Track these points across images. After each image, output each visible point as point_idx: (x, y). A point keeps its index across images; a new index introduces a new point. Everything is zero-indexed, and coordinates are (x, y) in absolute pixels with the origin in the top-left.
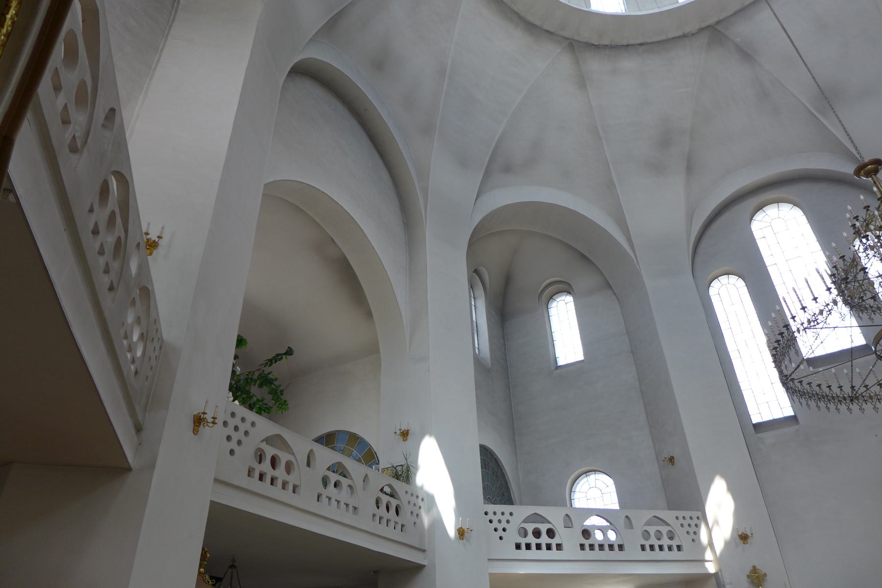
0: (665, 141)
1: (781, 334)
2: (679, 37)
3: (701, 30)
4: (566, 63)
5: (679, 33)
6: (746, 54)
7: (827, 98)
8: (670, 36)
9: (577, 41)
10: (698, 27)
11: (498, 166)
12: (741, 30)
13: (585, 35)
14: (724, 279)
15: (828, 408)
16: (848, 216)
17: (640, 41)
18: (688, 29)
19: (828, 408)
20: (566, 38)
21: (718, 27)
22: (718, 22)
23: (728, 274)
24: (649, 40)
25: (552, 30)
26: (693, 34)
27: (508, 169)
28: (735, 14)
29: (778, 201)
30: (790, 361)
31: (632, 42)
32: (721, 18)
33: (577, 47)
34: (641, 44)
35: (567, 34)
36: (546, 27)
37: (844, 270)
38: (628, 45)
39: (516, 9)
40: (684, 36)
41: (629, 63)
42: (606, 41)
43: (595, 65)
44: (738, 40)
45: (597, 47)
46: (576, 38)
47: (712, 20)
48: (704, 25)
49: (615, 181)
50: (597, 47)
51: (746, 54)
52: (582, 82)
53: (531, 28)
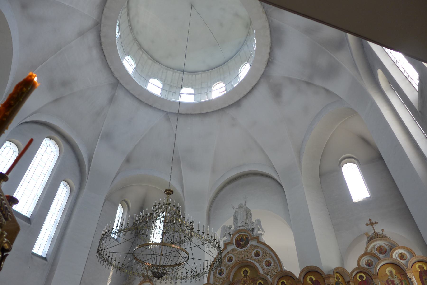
0: (65, 84)
1: (109, 230)
2: (111, 71)
4: (89, 23)
6: (112, 100)
7: (107, 136)
8: (111, 67)
9: (100, 26)
10: (117, 76)
12: (120, 93)
13: (104, 30)
14: (13, 145)
15: (106, 266)
17: (106, 55)
18: (115, 73)
19: (106, 266)
20: (101, 21)
21: (119, 84)
22: (121, 84)
23: (16, 145)
24: (107, 59)
28: (126, 89)
29: (57, 143)
30: (106, 241)
31: (105, 52)
33: (98, 26)
34: (104, 56)
35: (103, 20)
36: (105, 10)
38: (103, 50)
40: (112, 73)
41: (95, 53)
42: (103, 40)
43: (91, 38)
44: (116, 94)
45: (99, 36)
46: (102, 25)
47: (121, 81)
48: (119, 79)
50: (99, 36)
51: (112, 100)
52: (81, 34)
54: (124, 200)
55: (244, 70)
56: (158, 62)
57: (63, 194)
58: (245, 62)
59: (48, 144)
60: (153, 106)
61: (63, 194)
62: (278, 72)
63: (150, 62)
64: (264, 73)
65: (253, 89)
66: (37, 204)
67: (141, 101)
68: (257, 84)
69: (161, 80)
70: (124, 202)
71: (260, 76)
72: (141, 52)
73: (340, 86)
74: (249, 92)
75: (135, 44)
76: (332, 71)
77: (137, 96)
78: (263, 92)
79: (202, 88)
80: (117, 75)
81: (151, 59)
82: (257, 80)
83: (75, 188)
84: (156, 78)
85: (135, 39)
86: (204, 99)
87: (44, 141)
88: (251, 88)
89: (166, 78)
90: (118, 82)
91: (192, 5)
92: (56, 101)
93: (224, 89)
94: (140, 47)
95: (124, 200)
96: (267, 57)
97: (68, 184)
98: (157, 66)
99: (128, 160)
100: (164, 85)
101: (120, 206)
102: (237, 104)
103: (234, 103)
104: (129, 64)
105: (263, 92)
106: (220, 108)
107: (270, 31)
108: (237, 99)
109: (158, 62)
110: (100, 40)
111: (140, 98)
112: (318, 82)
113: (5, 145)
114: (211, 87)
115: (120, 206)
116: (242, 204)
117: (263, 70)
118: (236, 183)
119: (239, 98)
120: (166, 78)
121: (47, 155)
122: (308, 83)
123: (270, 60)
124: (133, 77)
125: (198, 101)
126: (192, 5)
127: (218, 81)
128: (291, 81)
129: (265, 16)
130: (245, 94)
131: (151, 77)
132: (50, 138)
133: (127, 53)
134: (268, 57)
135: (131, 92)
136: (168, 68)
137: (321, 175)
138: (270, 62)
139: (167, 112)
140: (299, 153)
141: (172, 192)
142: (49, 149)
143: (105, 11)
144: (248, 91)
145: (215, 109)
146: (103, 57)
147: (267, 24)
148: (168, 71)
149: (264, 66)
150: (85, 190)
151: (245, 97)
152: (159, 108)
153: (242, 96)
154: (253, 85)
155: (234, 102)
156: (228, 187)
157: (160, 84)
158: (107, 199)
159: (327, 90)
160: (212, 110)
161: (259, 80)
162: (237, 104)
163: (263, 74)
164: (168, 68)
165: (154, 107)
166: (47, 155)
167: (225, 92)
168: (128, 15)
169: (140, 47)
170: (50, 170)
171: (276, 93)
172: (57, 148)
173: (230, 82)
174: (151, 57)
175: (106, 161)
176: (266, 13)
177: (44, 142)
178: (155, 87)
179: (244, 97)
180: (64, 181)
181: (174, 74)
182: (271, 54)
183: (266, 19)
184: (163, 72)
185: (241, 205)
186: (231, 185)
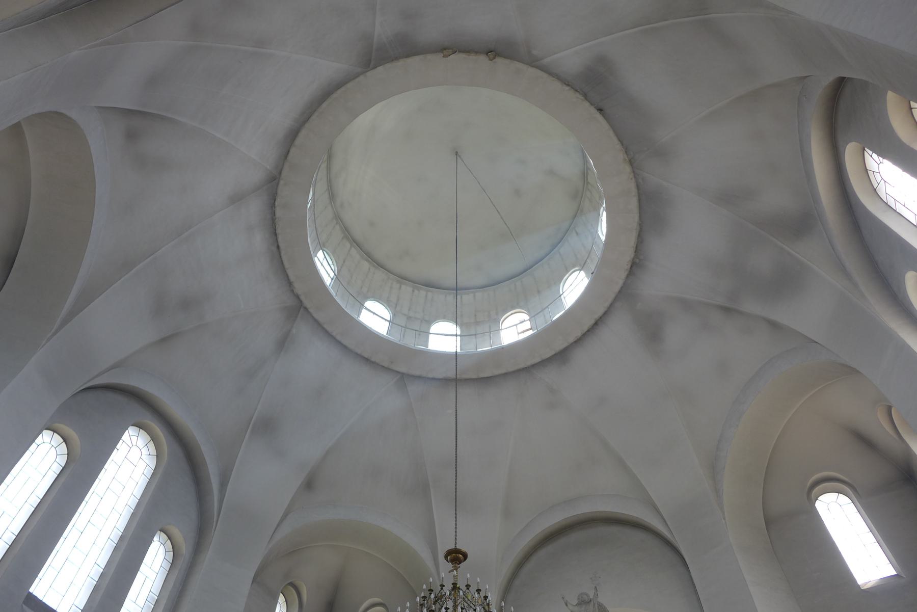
3: (298, 297)
5: (292, 278)
6: (283, 343)
9: (278, 184)
11: (136, 123)
13: (284, 192)
14: (57, 439)
16: (425, 587)
17: (281, 245)
20: (280, 173)
21: (302, 309)
22: (306, 309)
23: (65, 441)
24: (282, 254)
25: (289, 158)
26: (293, 291)
27: (131, 136)
28: (316, 320)
29: (154, 438)
31: (280, 238)
32: (311, 310)
33: (272, 183)
34: (278, 247)
35: (285, 173)
36: (293, 150)
37: (436, 597)
38: (276, 235)
39: (313, 117)
40: (290, 283)
41: (259, 240)
42: (279, 213)
43: (254, 208)
44: (294, 331)
46: (282, 182)
47: (306, 303)
48: (302, 298)
49: (133, 271)
50: (272, 206)
51: (283, 343)
52: (237, 199)
53: (293, 135)
54: (292, 584)
55: (574, 286)
56: (380, 265)
57: (156, 559)
58: (574, 267)
59: (134, 439)
60: (373, 360)
61: (156, 559)
62: (656, 286)
63: (366, 265)
64: (622, 288)
65: (596, 324)
66: (96, 589)
67: (345, 347)
68: (606, 313)
69: (387, 303)
70: (292, 588)
71: (613, 296)
72: (348, 245)
73: (808, 314)
74: (588, 331)
75: (338, 227)
76: (786, 281)
77: (338, 338)
78: (620, 329)
79: (477, 323)
80: (299, 288)
81: (367, 260)
82: (607, 304)
83: (186, 549)
84: (379, 299)
85: (338, 218)
86: (485, 348)
87: (126, 434)
88: (593, 322)
89: (398, 300)
90: (302, 306)
91: (457, 153)
92: (164, 340)
93: (528, 325)
94: (347, 234)
95: (292, 584)
96: (629, 255)
97: (169, 538)
98: (380, 275)
99: (309, 485)
100: (394, 315)
101: (281, 599)
102: (561, 357)
103: (555, 353)
104: (325, 267)
105: (620, 329)
106: (522, 366)
107: (640, 201)
108: (560, 345)
109: (380, 265)
110: (274, 214)
111: (346, 342)
112: (751, 306)
113: (39, 440)
114: (497, 321)
115: (281, 599)
116: (586, 594)
117: (621, 282)
118: (562, 541)
119: (565, 345)
120: (398, 300)
121: (131, 464)
122: (727, 310)
123: (637, 261)
124: (334, 294)
125: (542, 325)
126: (457, 153)
127: (513, 308)
128: (686, 305)
129: (628, 169)
130: (579, 334)
131: (367, 298)
132: (140, 426)
133: (322, 246)
134: (632, 256)
135: (325, 326)
136: (403, 279)
137: (769, 522)
138: (636, 266)
139: (403, 374)
140: (713, 468)
141: (465, 556)
142: (135, 450)
143: (291, 154)
144: (586, 328)
145: (511, 370)
146: (274, 248)
147: (633, 185)
148: (403, 287)
149: (623, 275)
150: (209, 555)
151: (578, 341)
152: (386, 364)
153: (572, 339)
154: (597, 316)
155: (553, 353)
156: (542, 553)
157: (387, 314)
158: (257, 579)
159: (774, 325)
160: (503, 371)
161: (611, 305)
162: (561, 357)
163: (620, 292)
164: (403, 279)
165: (374, 363)
166: (131, 464)
167: (531, 332)
168: (329, 169)
169: (347, 234)
170: (133, 502)
171: (652, 331)
172: (153, 451)
173: (542, 310)
174: (369, 256)
175: (261, 482)
176: (631, 162)
177: (126, 436)
178: (375, 317)
179: (575, 342)
180: (161, 530)
181: (416, 292)
182: (639, 248)
183: (632, 176)
184: (391, 288)
185: (585, 596)
186: (550, 548)
